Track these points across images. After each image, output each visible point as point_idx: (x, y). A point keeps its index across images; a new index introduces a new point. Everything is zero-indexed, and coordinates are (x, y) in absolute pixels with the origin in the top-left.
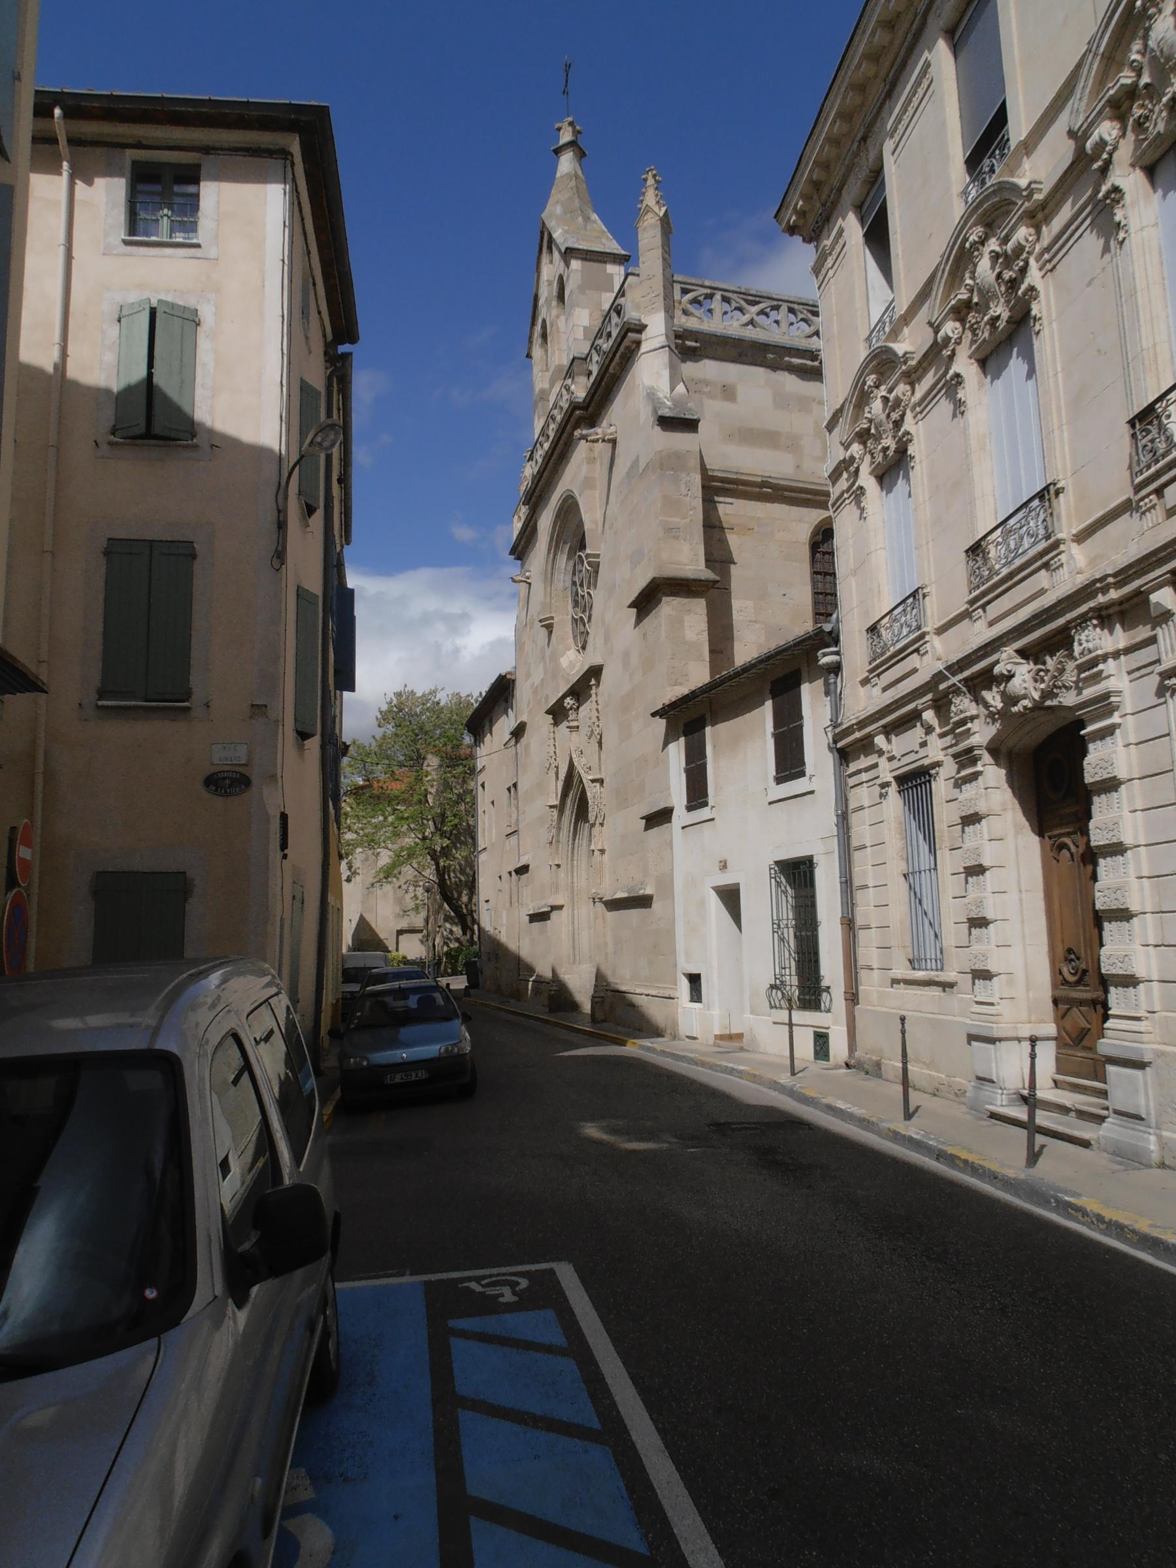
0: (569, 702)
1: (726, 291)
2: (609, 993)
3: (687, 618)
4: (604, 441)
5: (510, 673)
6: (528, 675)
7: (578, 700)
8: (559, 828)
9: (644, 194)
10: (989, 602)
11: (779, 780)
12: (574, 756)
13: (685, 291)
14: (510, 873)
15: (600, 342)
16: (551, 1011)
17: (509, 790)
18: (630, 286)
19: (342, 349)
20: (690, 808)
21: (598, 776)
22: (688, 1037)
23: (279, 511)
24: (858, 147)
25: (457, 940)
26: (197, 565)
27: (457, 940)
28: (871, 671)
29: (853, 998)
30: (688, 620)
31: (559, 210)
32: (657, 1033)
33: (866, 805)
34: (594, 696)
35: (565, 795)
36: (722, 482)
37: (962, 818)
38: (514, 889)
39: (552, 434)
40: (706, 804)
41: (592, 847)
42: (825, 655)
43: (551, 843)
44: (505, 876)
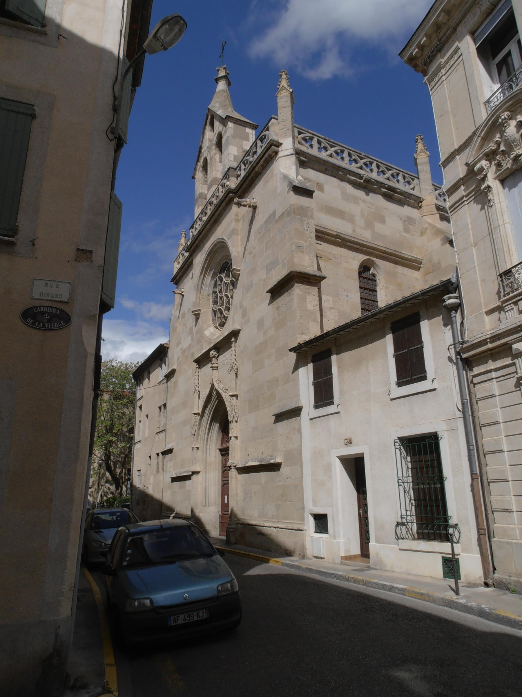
0: (213, 353)
1: (319, 137)
2: (239, 526)
3: (308, 297)
4: (250, 206)
5: (166, 344)
7: (218, 352)
8: (200, 426)
9: (280, 82)
11: (316, 407)
12: (215, 383)
13: (300, 133)
14: (158, 454)
17: (160, 408)
18: (273, 124)
21: (235, 393)
22: (315, 557)
23: (115, 98)
25: (112, 493)
26: (36, 125)
27: (112, 493)
30: (309, 298)
31: (217, 105)
32: (288, 553)
33: (497, 394)
34: (233, 348)
38: (161, 463)
39: (209, 212)
40: (332, 403)
42: (450, 298)
43: (194, 435)
44: (154, 456)
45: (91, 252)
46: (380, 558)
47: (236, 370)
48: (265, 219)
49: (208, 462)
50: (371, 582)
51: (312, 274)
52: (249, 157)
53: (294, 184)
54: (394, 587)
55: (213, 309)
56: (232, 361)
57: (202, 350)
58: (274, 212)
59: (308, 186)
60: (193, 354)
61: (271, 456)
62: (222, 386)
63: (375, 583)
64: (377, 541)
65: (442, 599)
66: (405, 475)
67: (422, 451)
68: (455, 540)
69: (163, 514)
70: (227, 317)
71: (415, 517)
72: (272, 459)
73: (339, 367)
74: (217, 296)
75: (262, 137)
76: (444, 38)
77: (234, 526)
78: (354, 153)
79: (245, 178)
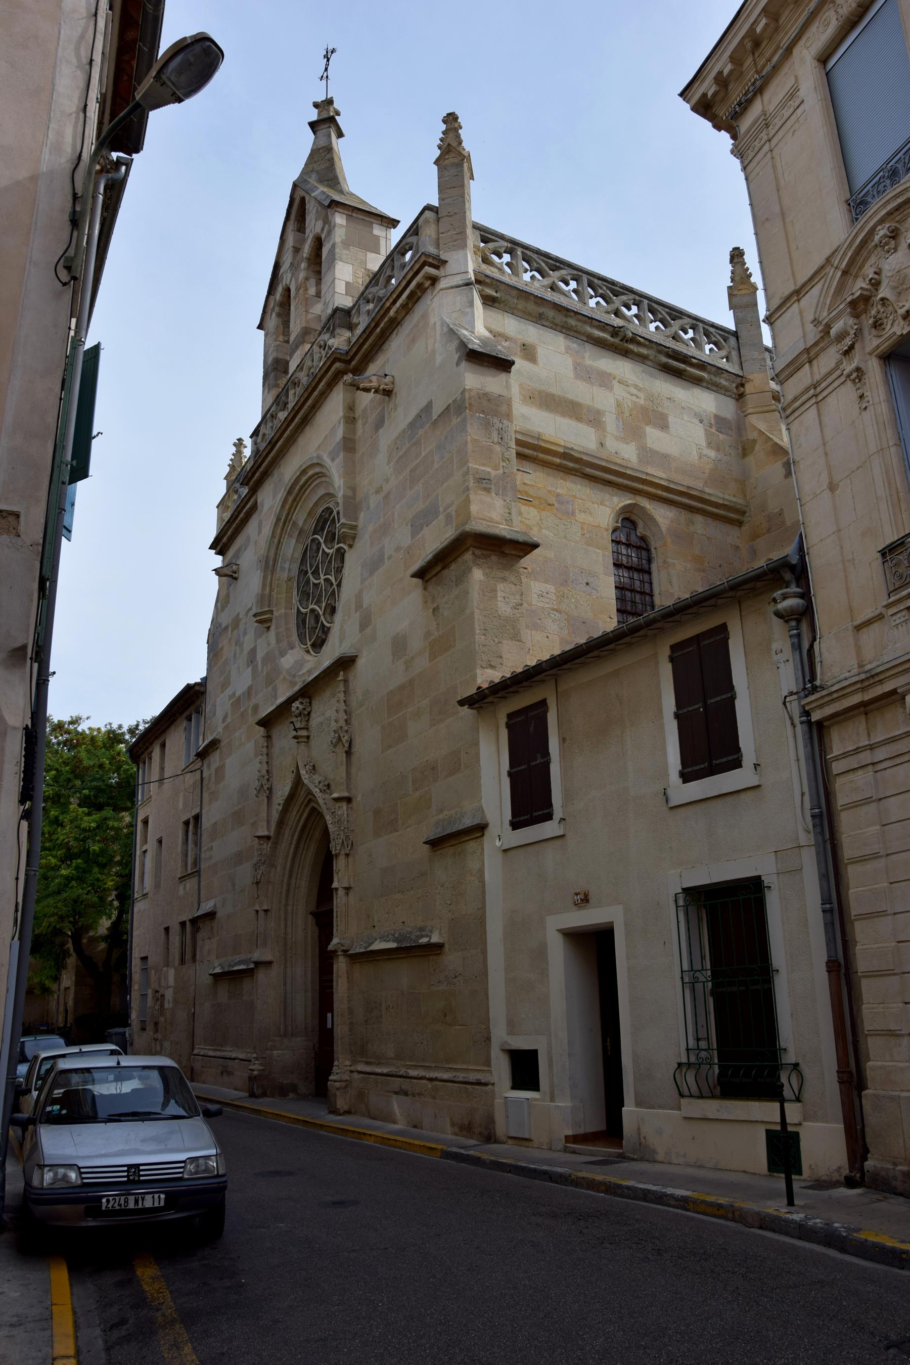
4: (376, 391)
11: (516, 825)
12: (303, 772)
16: (252, 1095)
18: (427, 221)
21: (346, 794)
22: (511, 1138)
23: (75, 197)
28: (888, 606)
36: (668, 356)
37: (683, 889)
41: (257, 908)
42: (785, 597)
44: (175, 929)
46: (645, 1138)
47: (347, 745)
48: (410, 418)
50: (619, 1186)
51: (508, 537)
52: (377, 288)
53: (470, 346)
54: (666, 1195)
55: (298, 610)
56: (339, 725)
57: (276, 699)
59: (502, 350)
60: (256, 708)
61: (421, 929)
62: (317, 778)
63: (628, 1188)
64: (639, 1103)
65: (758, 1214)
66: (697, 966)
67: (729, 917)
68: (787, 1093)
69: (195, 1052)
70: (329, 628)
71: (715, 1052)
72: (422, 936)
73: (563, 740)
74: (308, 581)
75: (403, 247)
76: (768, 68)
77: (346, 1077)
78: (600, 282)
79: (368, 332)
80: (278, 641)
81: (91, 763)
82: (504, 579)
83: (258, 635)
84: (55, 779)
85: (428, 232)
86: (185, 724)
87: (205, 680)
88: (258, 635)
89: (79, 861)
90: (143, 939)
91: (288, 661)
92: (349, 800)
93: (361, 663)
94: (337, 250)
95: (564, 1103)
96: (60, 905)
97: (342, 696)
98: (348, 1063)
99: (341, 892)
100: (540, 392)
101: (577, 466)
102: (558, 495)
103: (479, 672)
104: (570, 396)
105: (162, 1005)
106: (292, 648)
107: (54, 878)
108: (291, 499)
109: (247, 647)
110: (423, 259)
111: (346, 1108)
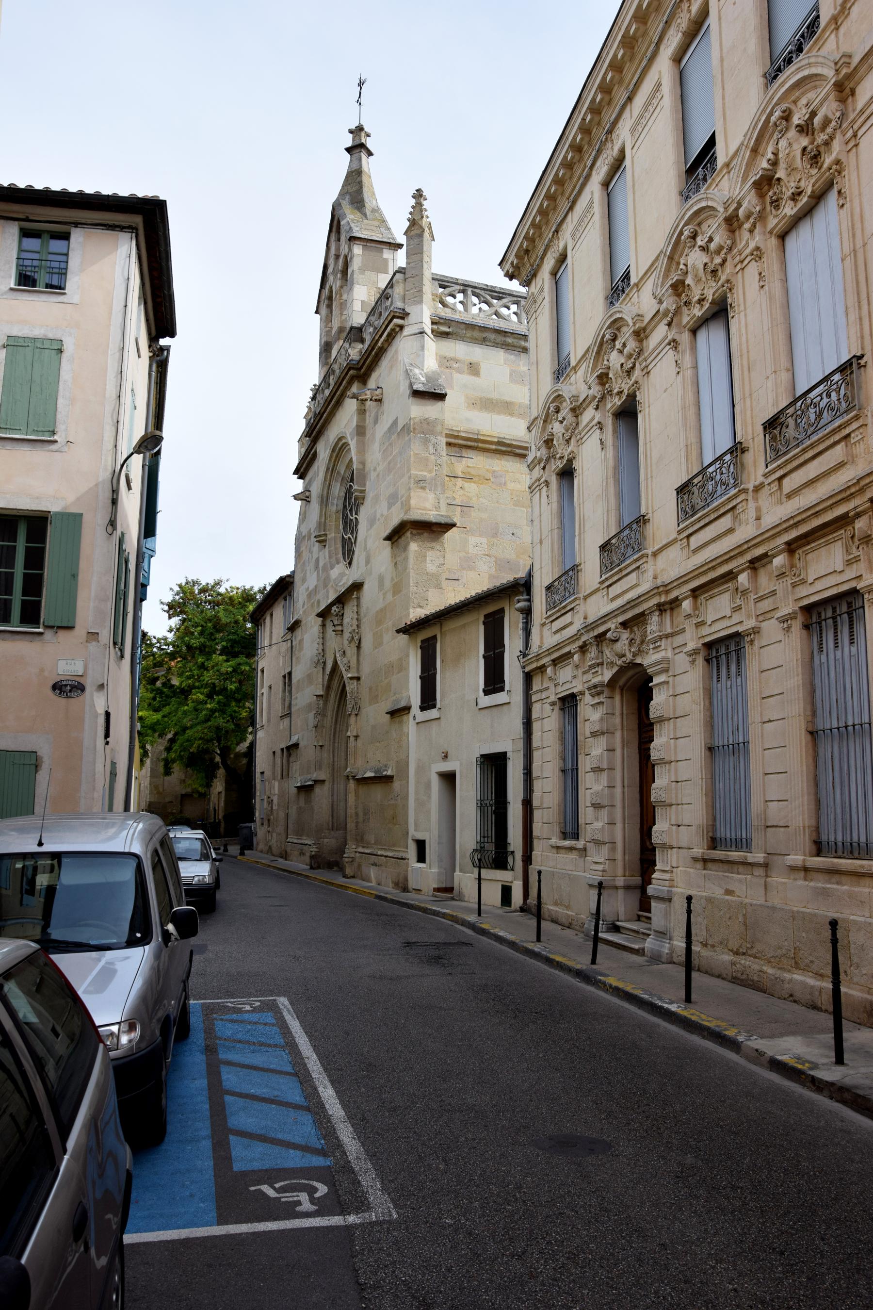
4: (371, 400)
6: (304, 580)
10: (610, 585)
11: (487, 692)
12: (338, 655)
15: (372, 318)
16: (312, 868)
19: (163, 342)
20: (422, 709)
21: (356, 675)
23: (113, 491)
24: (553, 236)
29: (527, 859)
35: (328, 688)
40: (434, 706)
42: (519, 601)
44: (278, 753)
45: (98, 634)
49: (336, 767)
51: (434, 521)
58: (396, 422)
62: (345, 660)
64: (461, 871)
73: (442, 661)
77: (352, 855)
80: (330, 557)
81: (228, 621)
82: (432, 548)
83: (320, 550)
84: (201, 633)
85: (398, 290)
86: (283, 602)
87: (293, 572)
88: (320, 550)
89: (220, 697)
90: (262, 761)
91: (334, 573)
92: (358, 679)
93: (366, 587)
94: (355, 276)
95: (435, 870)
96: (206, 731)
97: (355, 608)
98: (354, 847)
99: (352, 739)
100: (481, 399)
101: (509, 449)
102: (494, 472)
103: (411, 610)
104: (506, 398)
105: (272, 807)
106: (338, 563)
107: (202, 710)
108: (335, 455)
109: (315, 556)
110: (392, 314)
111: (352, 874)
